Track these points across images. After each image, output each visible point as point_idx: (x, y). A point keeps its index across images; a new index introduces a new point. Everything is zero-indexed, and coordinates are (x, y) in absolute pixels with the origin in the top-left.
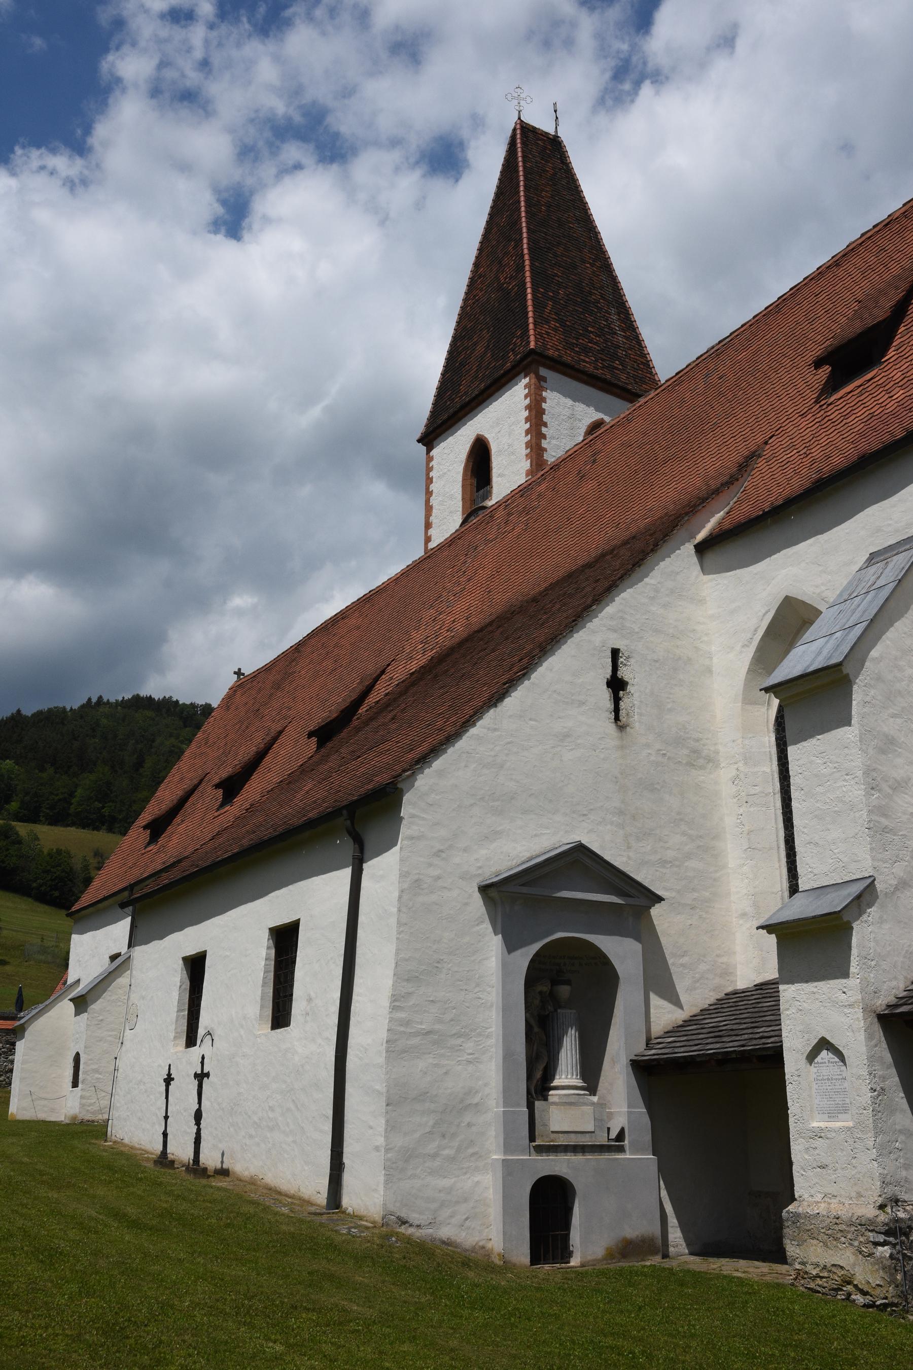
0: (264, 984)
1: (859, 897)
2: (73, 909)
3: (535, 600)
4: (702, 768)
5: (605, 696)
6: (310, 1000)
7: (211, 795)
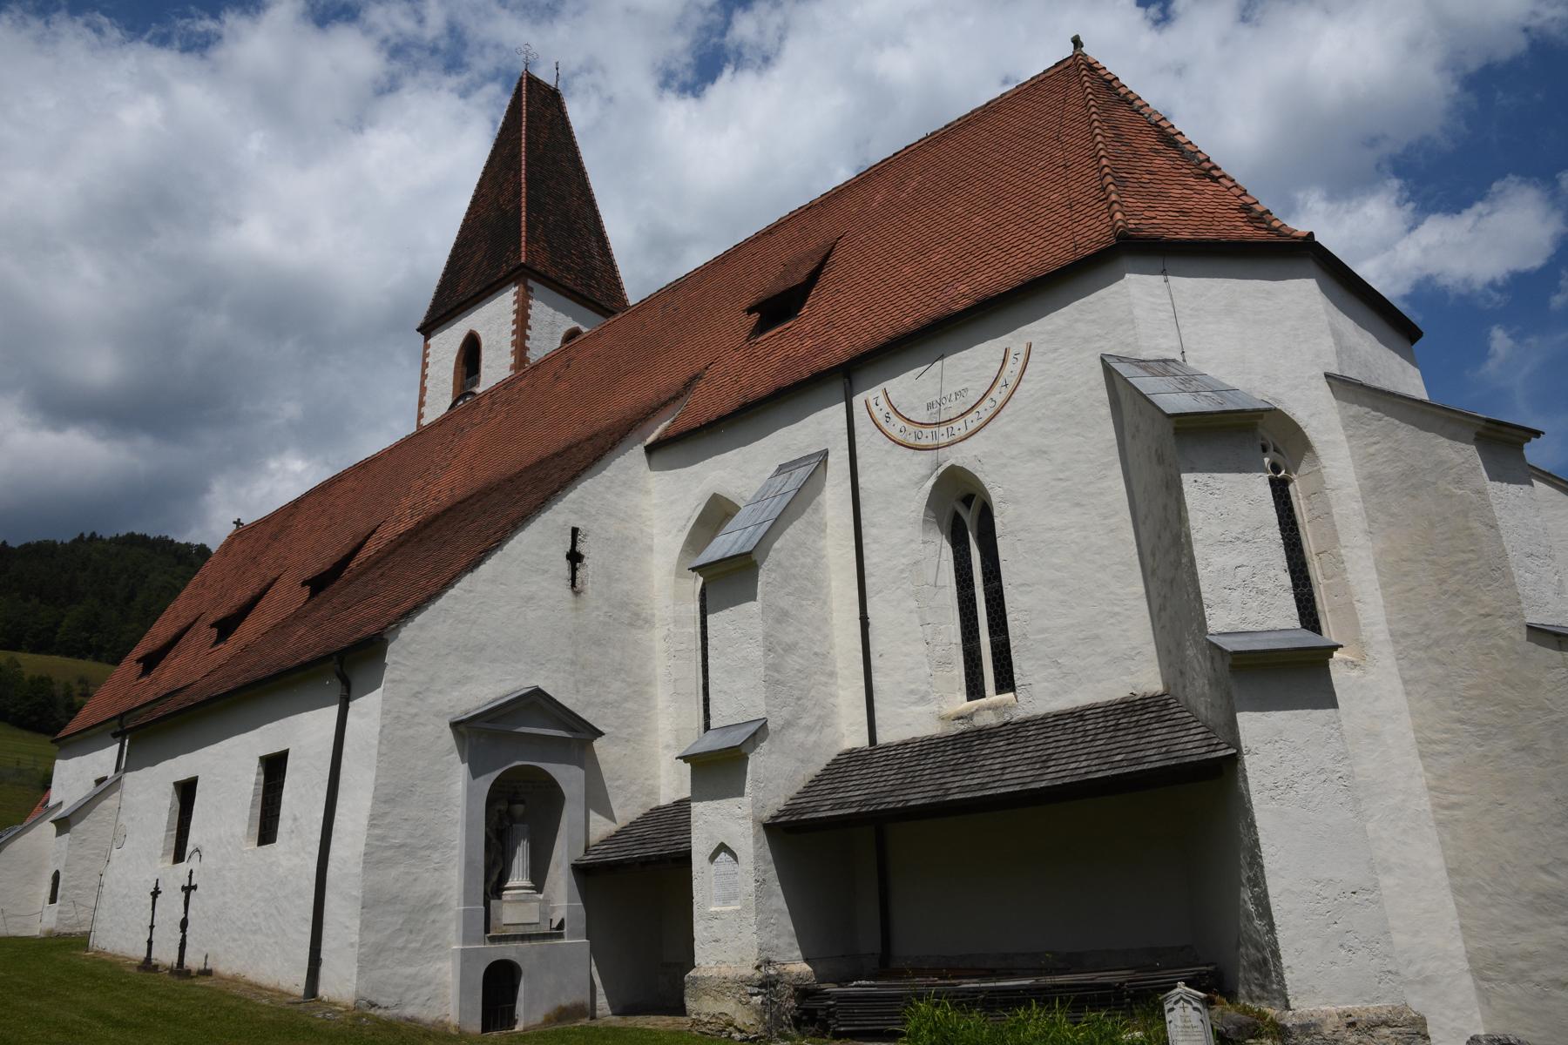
0: (253, 806)
1: (755, 734)
2: (60, 735)
3: (510, 480)
4: (641, 627)
5: (565, 565)
6: (295, 819)
7: (206, 633)
